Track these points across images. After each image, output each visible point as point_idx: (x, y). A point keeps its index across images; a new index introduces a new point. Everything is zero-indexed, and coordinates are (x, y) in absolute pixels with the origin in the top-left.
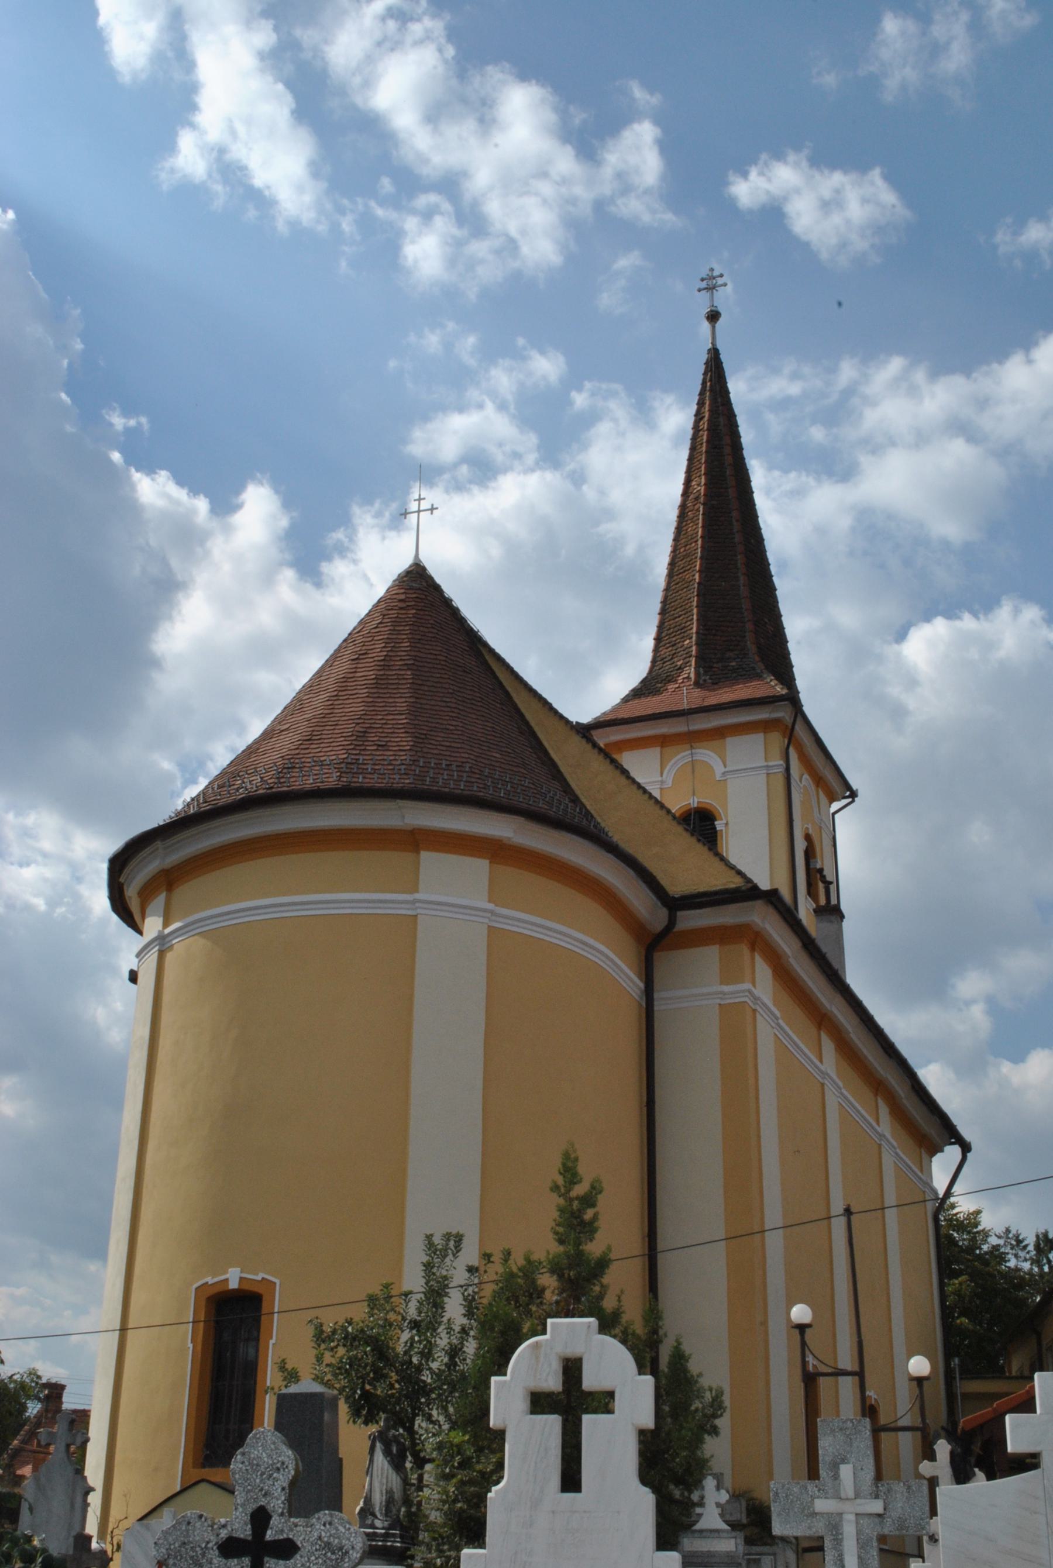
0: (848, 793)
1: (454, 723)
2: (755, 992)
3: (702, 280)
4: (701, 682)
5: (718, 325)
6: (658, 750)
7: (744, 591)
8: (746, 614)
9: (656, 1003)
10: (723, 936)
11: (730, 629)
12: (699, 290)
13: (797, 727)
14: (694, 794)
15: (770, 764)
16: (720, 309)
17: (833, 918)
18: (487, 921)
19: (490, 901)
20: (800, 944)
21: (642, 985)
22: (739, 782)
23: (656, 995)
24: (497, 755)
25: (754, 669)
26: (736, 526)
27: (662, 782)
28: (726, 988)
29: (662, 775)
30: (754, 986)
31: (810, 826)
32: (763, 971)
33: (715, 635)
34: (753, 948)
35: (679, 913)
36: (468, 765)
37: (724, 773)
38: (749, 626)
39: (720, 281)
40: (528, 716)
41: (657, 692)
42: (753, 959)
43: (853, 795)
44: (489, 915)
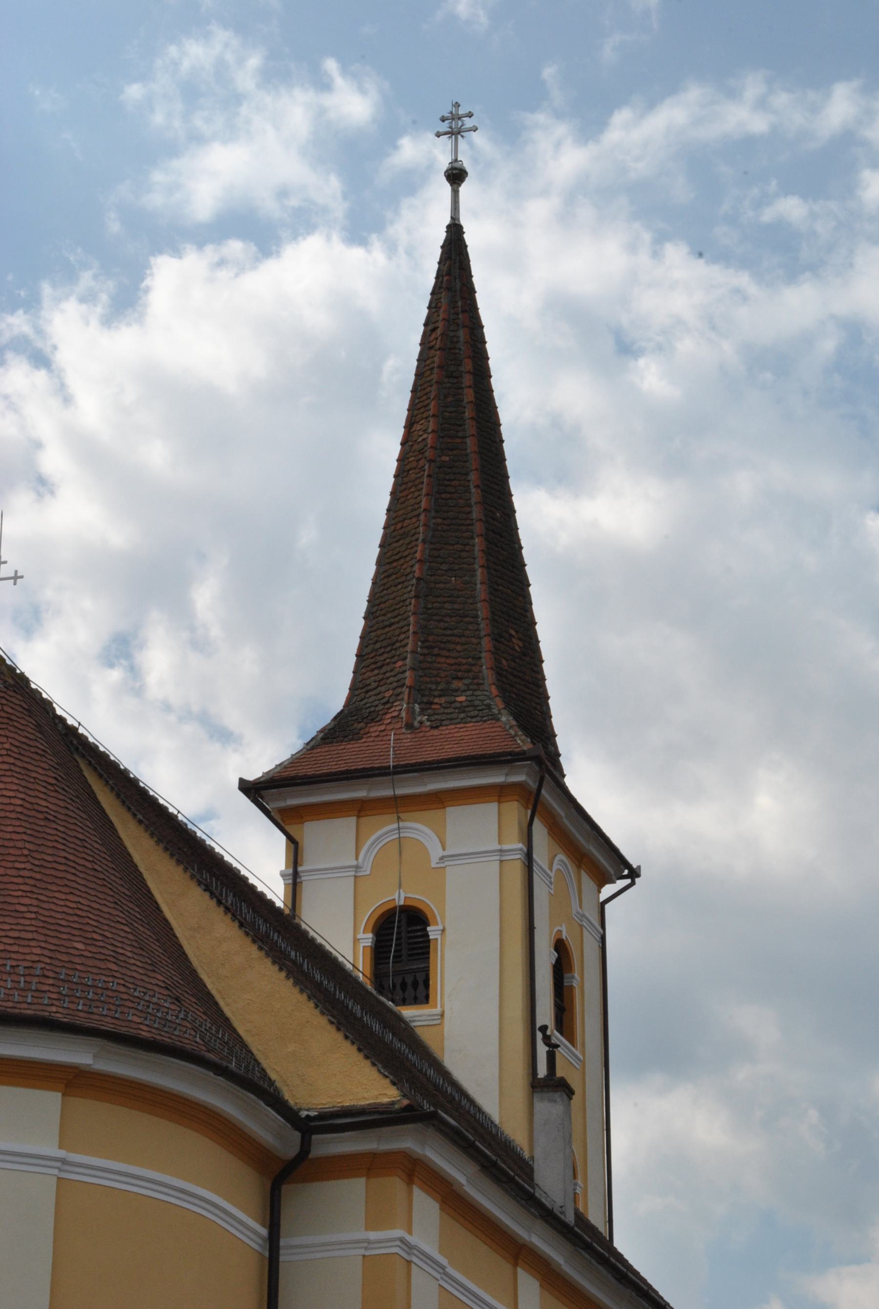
0: (626, 872)
1: (27, 901)
2: (412, 1239)
3: (443, 120)
4: (416, 724)
5: (463, 189)
6: (353, 820)
7: (481, 591)
8: (482, 626)
9: (281, 1252)
10: (370, 1165)
11: (459, 648)
12: (438, 135)
13: (543, 792)
14: (400, 886)
15: (506, 847)
16: (467, 165)
17: (557, 1096)
18: (56, 1172)
19: (60, 1147)
20: (478, 1168)
21: (264, 1232)
22: (463, 864)
23: (283, 1242)
24: (81, 946)
25: (489, 707)
26: (475, 495)
27: (357, 867)
28: (373, 1235)
29: (357, 858)
30: (410, 1232)
31: (564, 929)
32: (426, 1207)
33: (438, 655)
34: (410, 1180)
35: (314, 1137)
36: (40, 965)
37: (442, 858)
38: (486, 643)
39: (468, 123)
40: (137, 858)
41: (356, 736)
42: (410, 1193)
43: (634, 874)
44: (58, 1164)
